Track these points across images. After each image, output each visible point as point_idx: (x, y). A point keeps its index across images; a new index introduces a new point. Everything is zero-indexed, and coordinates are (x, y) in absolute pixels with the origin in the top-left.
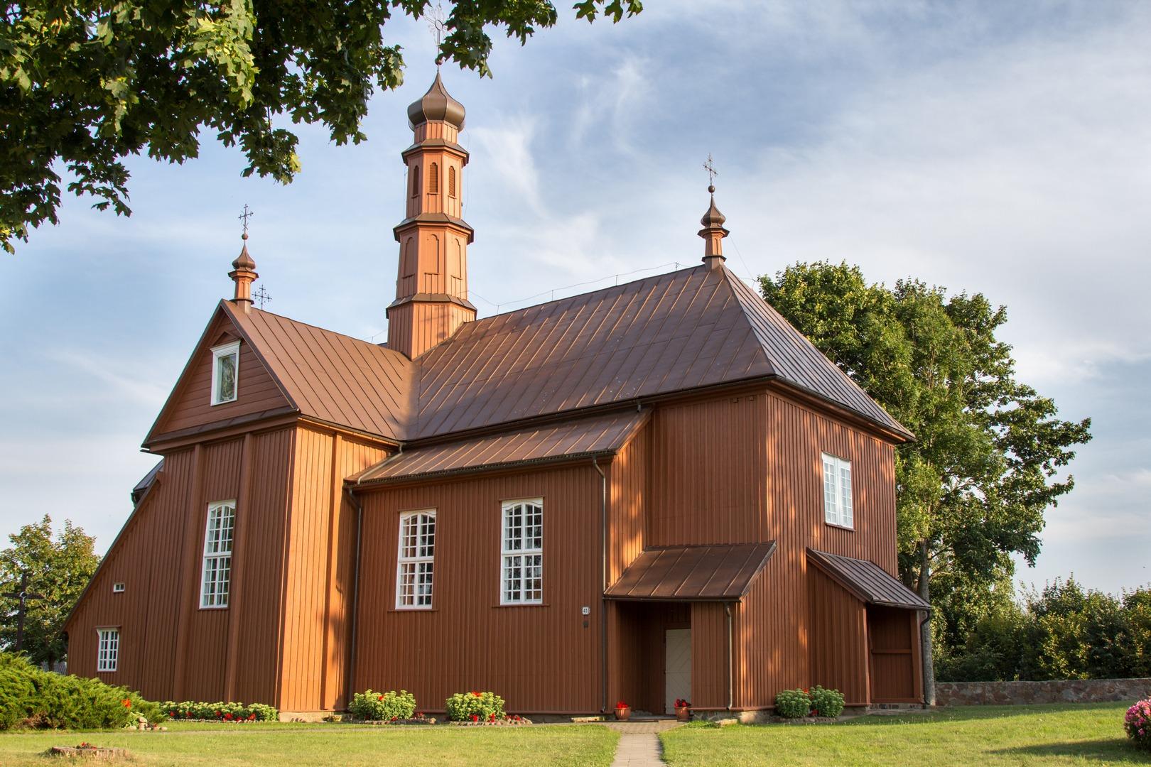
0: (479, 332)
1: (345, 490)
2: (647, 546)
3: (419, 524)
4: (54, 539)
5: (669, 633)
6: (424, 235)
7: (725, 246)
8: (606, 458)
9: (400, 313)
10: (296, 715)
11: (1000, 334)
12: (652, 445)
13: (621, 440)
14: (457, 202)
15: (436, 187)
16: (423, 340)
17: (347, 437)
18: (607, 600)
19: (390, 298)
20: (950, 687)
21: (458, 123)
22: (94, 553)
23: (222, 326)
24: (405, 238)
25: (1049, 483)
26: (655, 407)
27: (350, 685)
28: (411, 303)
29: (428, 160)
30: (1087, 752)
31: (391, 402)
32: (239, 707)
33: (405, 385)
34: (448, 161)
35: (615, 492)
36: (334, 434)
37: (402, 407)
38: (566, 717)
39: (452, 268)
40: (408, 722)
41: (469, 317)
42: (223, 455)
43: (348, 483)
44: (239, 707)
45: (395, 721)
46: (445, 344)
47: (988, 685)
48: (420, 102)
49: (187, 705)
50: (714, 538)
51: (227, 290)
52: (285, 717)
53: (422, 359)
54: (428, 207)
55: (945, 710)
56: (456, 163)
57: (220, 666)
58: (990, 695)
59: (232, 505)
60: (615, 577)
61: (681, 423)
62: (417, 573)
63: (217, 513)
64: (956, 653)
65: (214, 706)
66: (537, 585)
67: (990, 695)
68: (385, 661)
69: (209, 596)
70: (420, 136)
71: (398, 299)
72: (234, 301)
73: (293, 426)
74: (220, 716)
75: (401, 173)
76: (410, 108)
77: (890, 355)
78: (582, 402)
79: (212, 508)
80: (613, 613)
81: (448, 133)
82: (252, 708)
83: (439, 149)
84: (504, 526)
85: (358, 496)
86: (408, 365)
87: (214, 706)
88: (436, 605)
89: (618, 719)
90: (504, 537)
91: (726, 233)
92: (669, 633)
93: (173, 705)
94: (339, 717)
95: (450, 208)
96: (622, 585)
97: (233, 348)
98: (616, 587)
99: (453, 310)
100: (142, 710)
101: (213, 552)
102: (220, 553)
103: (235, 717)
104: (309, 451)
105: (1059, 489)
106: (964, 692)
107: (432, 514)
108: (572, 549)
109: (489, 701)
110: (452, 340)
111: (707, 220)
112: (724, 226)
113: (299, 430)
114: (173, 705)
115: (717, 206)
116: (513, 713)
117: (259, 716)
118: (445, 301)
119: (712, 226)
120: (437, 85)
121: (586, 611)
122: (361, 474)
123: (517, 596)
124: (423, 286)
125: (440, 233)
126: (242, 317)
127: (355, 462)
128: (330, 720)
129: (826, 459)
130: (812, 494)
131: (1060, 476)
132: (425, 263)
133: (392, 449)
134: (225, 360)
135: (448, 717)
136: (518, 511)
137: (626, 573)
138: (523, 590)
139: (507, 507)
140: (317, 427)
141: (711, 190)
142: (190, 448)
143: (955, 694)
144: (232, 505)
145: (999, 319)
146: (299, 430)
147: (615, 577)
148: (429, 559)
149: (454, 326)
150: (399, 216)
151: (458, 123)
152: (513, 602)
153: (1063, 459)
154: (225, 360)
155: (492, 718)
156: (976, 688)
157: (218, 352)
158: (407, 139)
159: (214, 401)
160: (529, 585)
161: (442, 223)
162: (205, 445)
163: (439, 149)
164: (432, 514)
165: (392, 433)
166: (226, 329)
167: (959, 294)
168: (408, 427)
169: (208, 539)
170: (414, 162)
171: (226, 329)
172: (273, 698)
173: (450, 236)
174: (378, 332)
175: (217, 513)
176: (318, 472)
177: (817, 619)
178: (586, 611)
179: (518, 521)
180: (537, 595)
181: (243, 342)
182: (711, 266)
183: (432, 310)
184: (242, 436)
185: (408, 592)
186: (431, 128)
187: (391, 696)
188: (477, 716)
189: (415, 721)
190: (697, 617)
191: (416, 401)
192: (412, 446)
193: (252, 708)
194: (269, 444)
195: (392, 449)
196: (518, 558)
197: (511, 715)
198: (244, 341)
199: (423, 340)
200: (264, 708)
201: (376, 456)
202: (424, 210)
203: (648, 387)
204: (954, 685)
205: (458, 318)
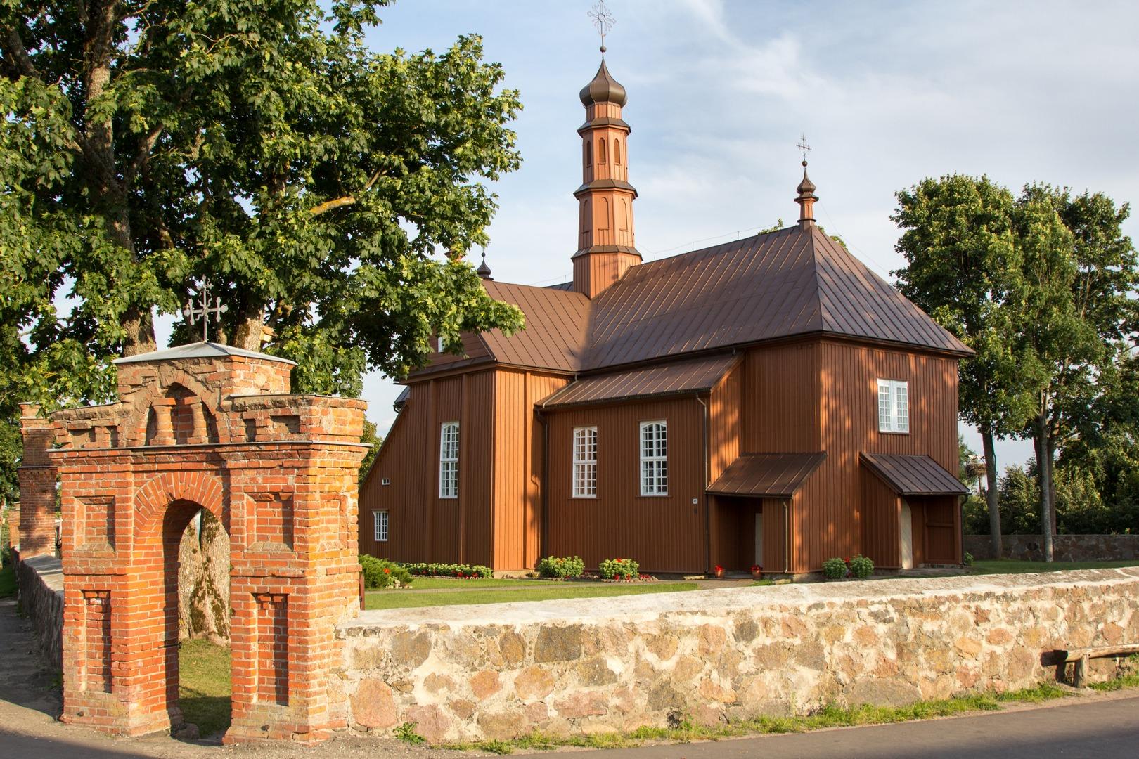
0: (645, 275)
1: (535, 412)
2: (743, 452)
3: (587, 437)
6: (596, 199)
7: (816, 210)
9: (581, 260)
10: (506, 573)
11: (1125, 229)
12: (745, 375)
13: (721, 374)
14: (622, 168)
15: (604, 159)
16: (599, 282)
17: (533, 373)
18: (709, 495)
19: (574, 249)
20: (1069, 539)
21: (620, 101)
22: (377, 435)
26: (745, 352)
27: (544, 552)
28: (588, 255)
29: (597, 136)
31: (569, 335)
33: (583, 323)
34: (613, 135)
36: (525, 372)
37: (579, 340)
40: (576, 580)
41: (635, 261)
42: (449, 388)
43: (537, 408)
45: (567, 579)
46: (616, 284)
47: (1102, 538)
49: (433, 566)
50: (783, 446)
52: (497, 575)
53: (598, 298)
54: (599, 174)
55: (1063, 561)
58: (1103, 546)
60: (716, 474)
61: (766, 363)
62: (586, 472)
64: (1115, 501)
65: (451, 567)
67: (1103, 546)
69: (446, 489)
70: (590, 116)
71: (580, 250)
73: (494, 370)
74: (455, 574)
77: (1003, 260)
79: (444, 426)
80: (712, 505)
81: (612, 111)
82: (475, 568)
83: (605, 126)
85: (544, 415)
86: (587, 303)
87: (451, 567)
91: (817, 199)
93: (425, 566)
94: (537, 574)
95: (616, 174)
98: (717, 483)
100: (397, 575)
103: (465, 574)
104: (507, 388)
106: (1081, 543)
108: (687, 455)
109: (626, 564)
110: (621, 282)
112: (815, 194)
113: (498, 373)
114: (425, 566)
115: (810, 177)
116: (645, 572)
117: (479, 574)
118: (614, 251)
119: (805, 194)
120: (602, 71)
122: (546, 399)
124: (597, 240)
125: (608, 196)
127: (542, 390)
128: (530, 576)
129: (881, 383)
130: (867, 408)
132: (598, 221)
133: (570, 378)
135: (602, 576)
136: (651, 429)
141: (804, 164)
142: (427, 382)
143: (1074, 545)
144: (457, 425)
145: (1120, 218)
146: (498, 373)
147: (716, 474)
149: (622, 270)
150: (578, 183)
151: (620, 101)
155: (629, 577)
156: (1090, 540)
161: (609, 187)
162: (436, 380)
164: (595, 429)
165: (570, 365)
167: (1082, 195)
168: (584, 356)
169: (443, 448)
170: (588, 137)
172: (488, 561)
173: (617, 198)
175: (447, 434)
176: (514, 400)
177: (867, 505)
178: (695, 501)
180: (665, 489)
182: (804, 228)
184: (460, 376)
185: (581, 487)
186: (598, 108)
187: (567, 562)
188: (619, 576)
189: (583, 579)
190: (766, 507)
191: (590, 337)
192: (585, 375)
194: (479, 380)
195: (570, 378)
199: (599, 282)
200: (482, 568)
201: (561, 383)
202: (596, 178)
204: (1073, 536)
205: (625, 262)
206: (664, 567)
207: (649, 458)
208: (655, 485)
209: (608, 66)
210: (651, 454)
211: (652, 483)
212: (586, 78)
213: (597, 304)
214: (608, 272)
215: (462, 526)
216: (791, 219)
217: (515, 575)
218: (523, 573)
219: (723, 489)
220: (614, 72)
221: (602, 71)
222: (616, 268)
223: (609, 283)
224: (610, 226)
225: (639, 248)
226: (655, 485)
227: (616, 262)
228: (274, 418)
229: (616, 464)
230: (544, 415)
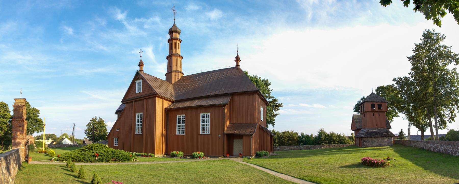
0: (184, 79)
4: (97, 120)
5: (235, 140)
6: (173, 58)
8: (225, 105)
16: (174, 79)
17: (165, 100)
18: (224, 134)
21: (179, 33)
23: (138, 76)
24: (169, 59)
25: (275, 113)
26: (232, 95)
28: (171, 72)
29: (174, 41)
30: (378, 163)
32: (146, 154)
35: (226, 111)
36: (163, 99)
38: (216, 157)
39: (179, 65)
44: (146, 154)
48: (172, 28)
51: (138, 69)
53: (174, 84)
54: (174, 52)
56: (179, 42)
57: (144, 146)
59: (142, 114)
60: (226, 129)
61: (237, 99)
63: (138, 115)
65: (141, 154)
66: (208, 130)
68: (181, 145)
69: (138, 131)
72: (140, 71)
73: (156, 97)
74: (142, 156)
75: (167, 45)
76: (169, 30)
78: (216, 93)
79: (137, 114)
81: (177, 36)
82: (150, 154)
84: (177, 120)
87: (141, 154)
88: (211, 132)
89: (226, 157)
90: (177, 122)
92: (235, 140)
96: (227, 131)
97: (140, 81)
99: (180, 74)
101: (138, 123)
102: (139, 123)
103: (146, 156)
104: (159, 101)
105: (277, 115)
107: (184, 115)
108: (216, 124)
111: (140, 63)
113: (157, 99)
116: (206, 156)
117: (151, 156)
118: (178, 72)
120: (174, 25)
121: (220, 136)
123: (204, 132)
124: (174, 69)
126: (141, 73)
127: (167, 104)
131: (277, 113)
134: (138, 83)
135: (193, 157)
137: (227, 128)
138: (205, 131)
139: (178, 116)
140: (162, 98)
142: (132, 102)
147: (226, 129)
148: (184, 124)
149: (180, 77)
150: (167, 54)
151: (179, 33)
152: (203, 134)
153: (278, 110)
154: (138, 83)
157: (137, 82)
158: (168, 37)
159: (137, 92)
160: (206, 130)
161: (177, 55)
163: (176, 39)
165: (173, 99)
166: (139, 77)
170: (170, 42)
171: (139, 77)
172: (153, 152)
173: (179, 58)
174: (164, 78)
175: (138, 115)
176: (160, 106)
179: (180, 119)
181: (143, 79)
183: (176, 74)
184: (144, 99)
188: (199, 157)
189: (184, 158)
190: (244, 137)
192: (177, 101)
193: (150, 154)
194: (151, 100)
195: (173, 102)
196: (180, 126)
197: (206, 156)
198: (143, 79)
199: (174, 79)
203: (231, 91)
205: (181, 75)
206: (211, 153)
207: (203, 124)
208: (181, 132)
209: (176, 24)
210: (204, 122)
211: (180, 131)
212: (171, 26)
213: (175, 85)
214: (177, 77)
215: (144, 142)
216: (233, 65)
217: (160, 156)
218: (162, 155)
219: (228, 132)
220: (177, 25)
221: (174, 25)
222: (178, 77)
223: (177, 80)
224: (177, 65)
225: (183, 72)
226: (181, 132)
227: (178, 75)
228: (10, 174)
229: (192, 125)
230: (167, 111)
